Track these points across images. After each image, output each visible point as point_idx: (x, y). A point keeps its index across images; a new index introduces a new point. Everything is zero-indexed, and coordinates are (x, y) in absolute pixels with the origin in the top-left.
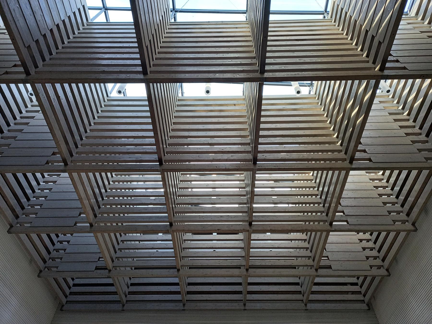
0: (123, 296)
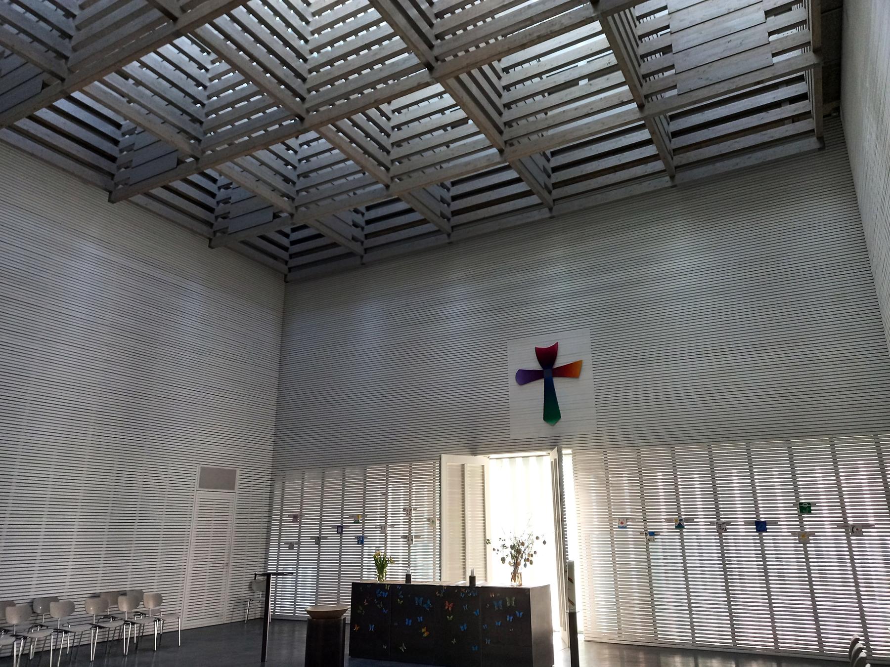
0: (545, 194)
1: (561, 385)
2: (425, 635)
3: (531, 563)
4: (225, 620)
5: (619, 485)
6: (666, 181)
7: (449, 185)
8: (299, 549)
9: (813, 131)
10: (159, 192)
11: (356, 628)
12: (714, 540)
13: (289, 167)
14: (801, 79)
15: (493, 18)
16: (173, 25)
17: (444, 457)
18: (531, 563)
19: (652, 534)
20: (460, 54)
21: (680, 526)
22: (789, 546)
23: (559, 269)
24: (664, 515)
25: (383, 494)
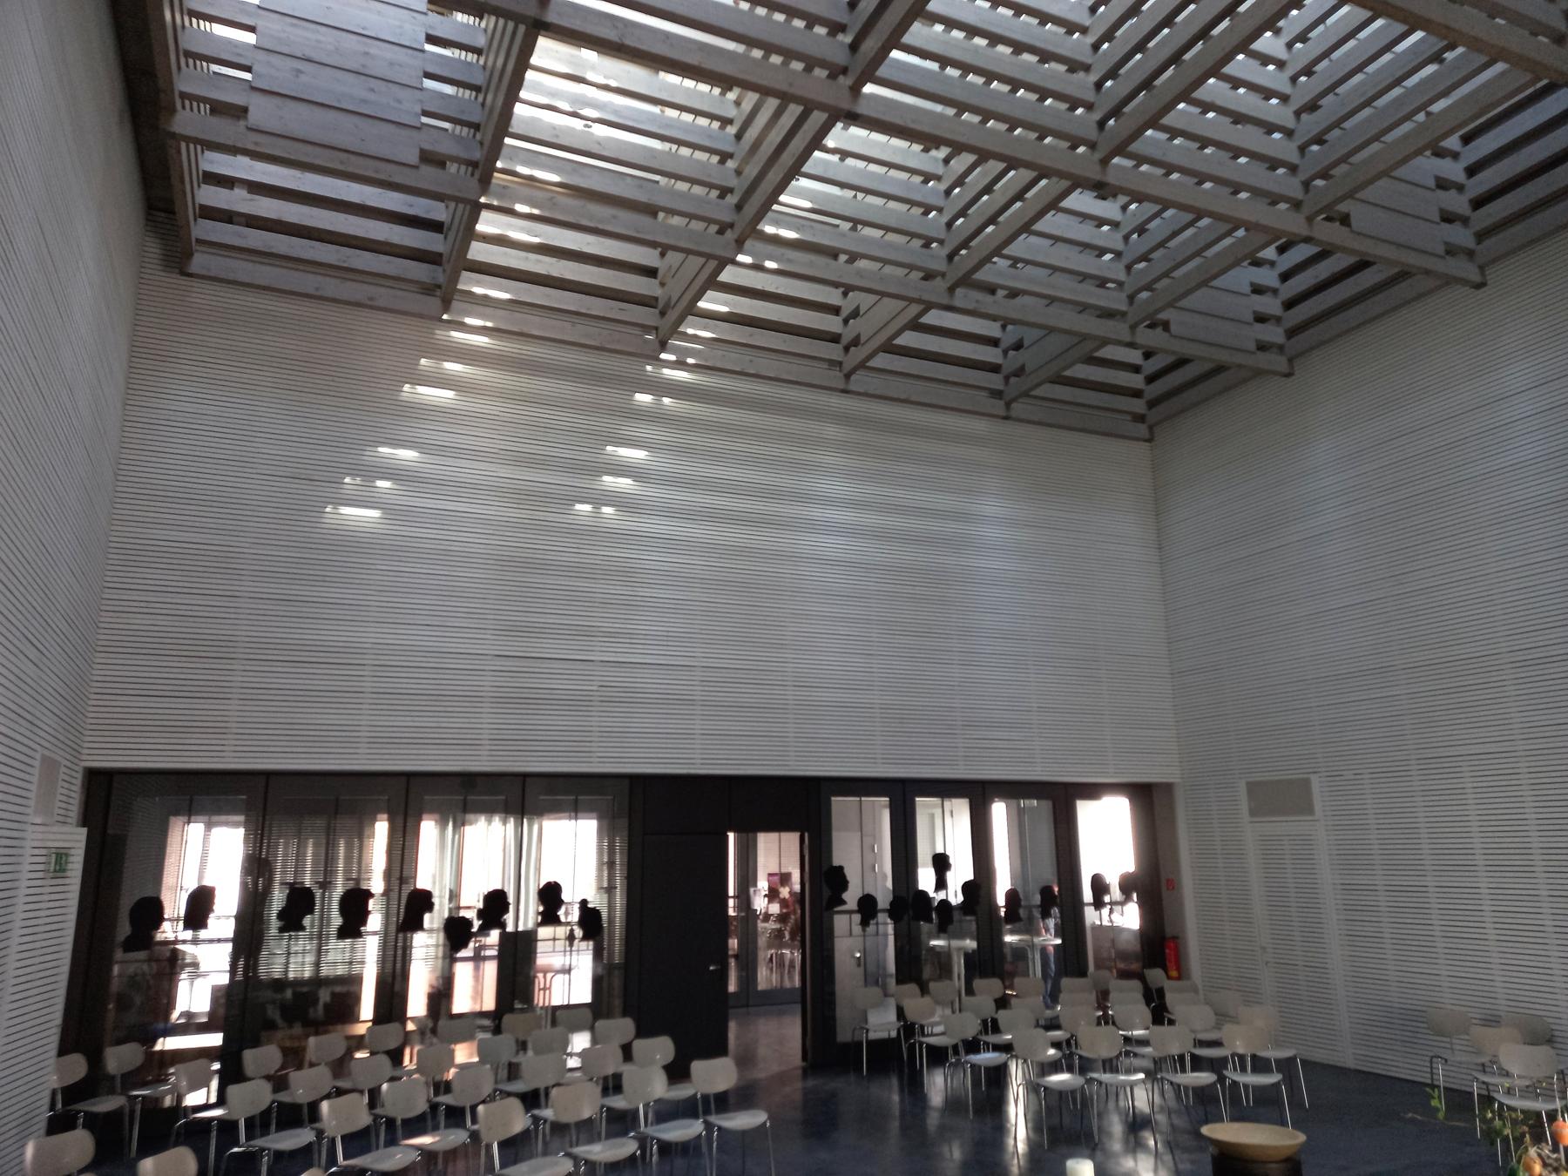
13: (1277, 136)
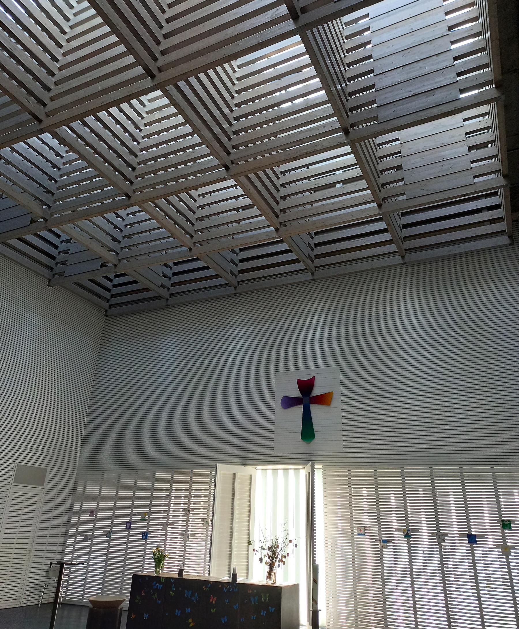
1: (316, 410)
2: (191, 625)
3: (284, 564)
4: (22, 603)
5: (359, 497)
6: (398, 259)
7: (238, 251)
8: (92, 541)
9: (505, 231)
10: (14, 242)
11: (133, 616)
12: (435, 548)
14: (496, 194)
15: (276, 137)
16: (38, 124)
17: (219, 465)
18: (284, 564)
19: (385, 541)
20: (266, 155)
21: (407, 536)
22: (495, 557)
23: (318, 319)
24: (395, 525)
25: (167, 496)
